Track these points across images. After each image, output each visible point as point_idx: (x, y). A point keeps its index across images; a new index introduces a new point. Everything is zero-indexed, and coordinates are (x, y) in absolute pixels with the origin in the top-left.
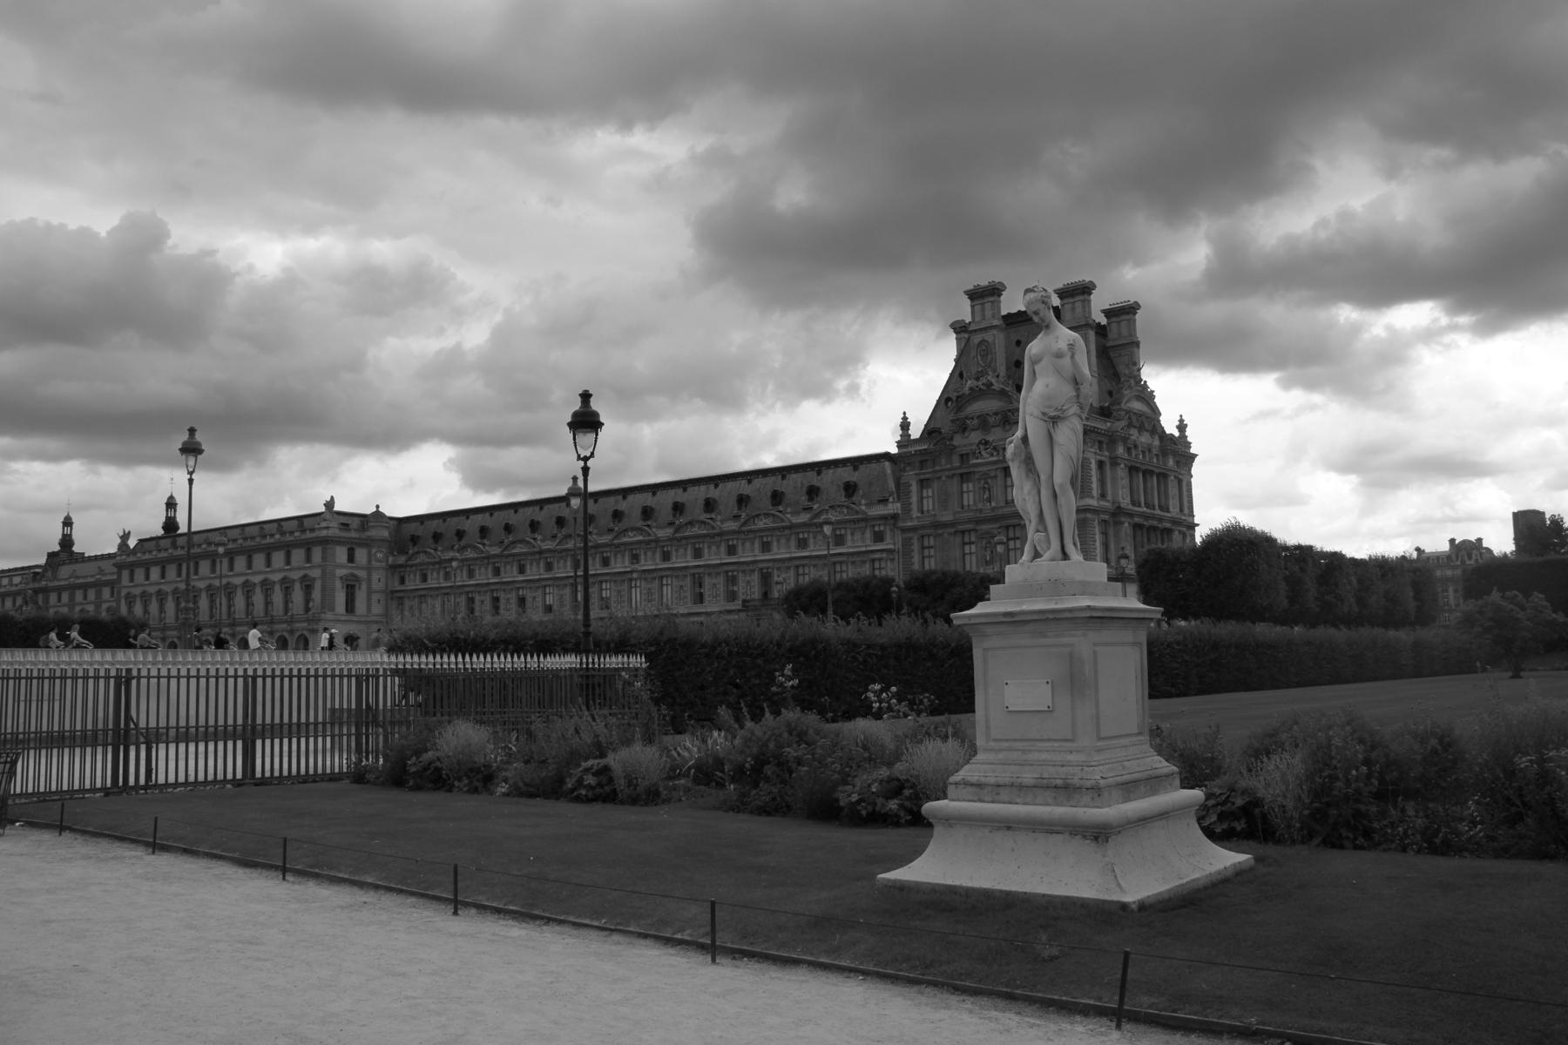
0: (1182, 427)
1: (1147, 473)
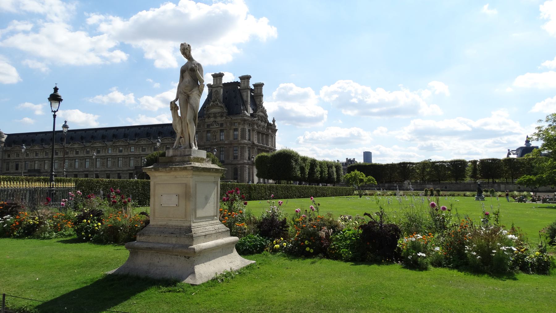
0: (274, 121)
1: (263, 134)
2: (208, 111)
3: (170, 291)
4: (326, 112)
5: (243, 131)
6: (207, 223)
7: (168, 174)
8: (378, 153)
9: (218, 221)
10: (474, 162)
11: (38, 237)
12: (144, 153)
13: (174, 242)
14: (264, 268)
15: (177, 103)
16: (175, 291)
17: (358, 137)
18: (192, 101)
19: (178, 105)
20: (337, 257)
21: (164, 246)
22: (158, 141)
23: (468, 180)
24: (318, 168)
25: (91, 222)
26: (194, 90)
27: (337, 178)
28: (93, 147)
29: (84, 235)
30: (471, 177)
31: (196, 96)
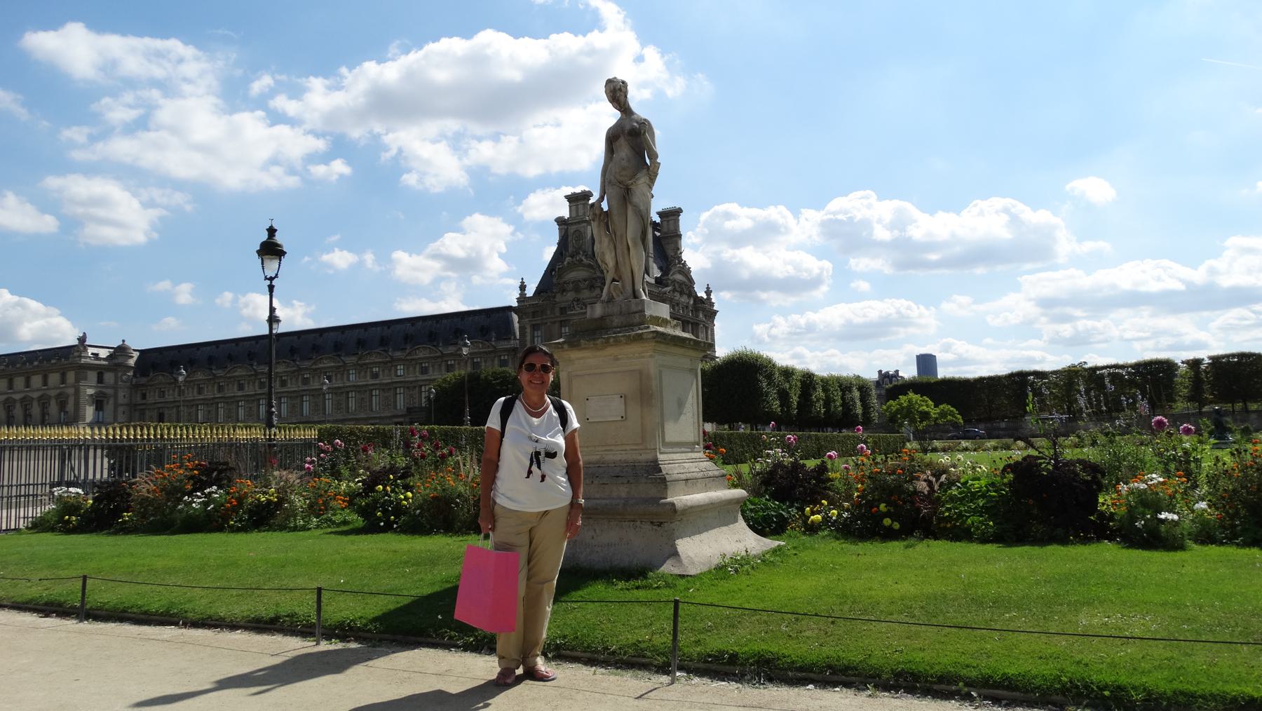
0: (708, 292)
2: (560, 276)
3: (638, 588)
4: (827, 264)
6: (683, 456)
7: (600, 353)
8: (949, 356)
9: (701, 455)
10: (1195, 364)
11: (283, 528)
12: (425, 377)
13: (623, 495)
14: (806, 556)
16: (645, 587)
17: (903, 321)
18: (636, 199)
20: (960, 534)
21: (604, 502)
22: (465, 345)
23: (1180, 406)
24: (820, 392)
25: (393, 491)
26: (639, 175)
27: (864, 414)
28: (315, 370)
29: (377, 517)
30: (1191, 399)
31: (645, 188)
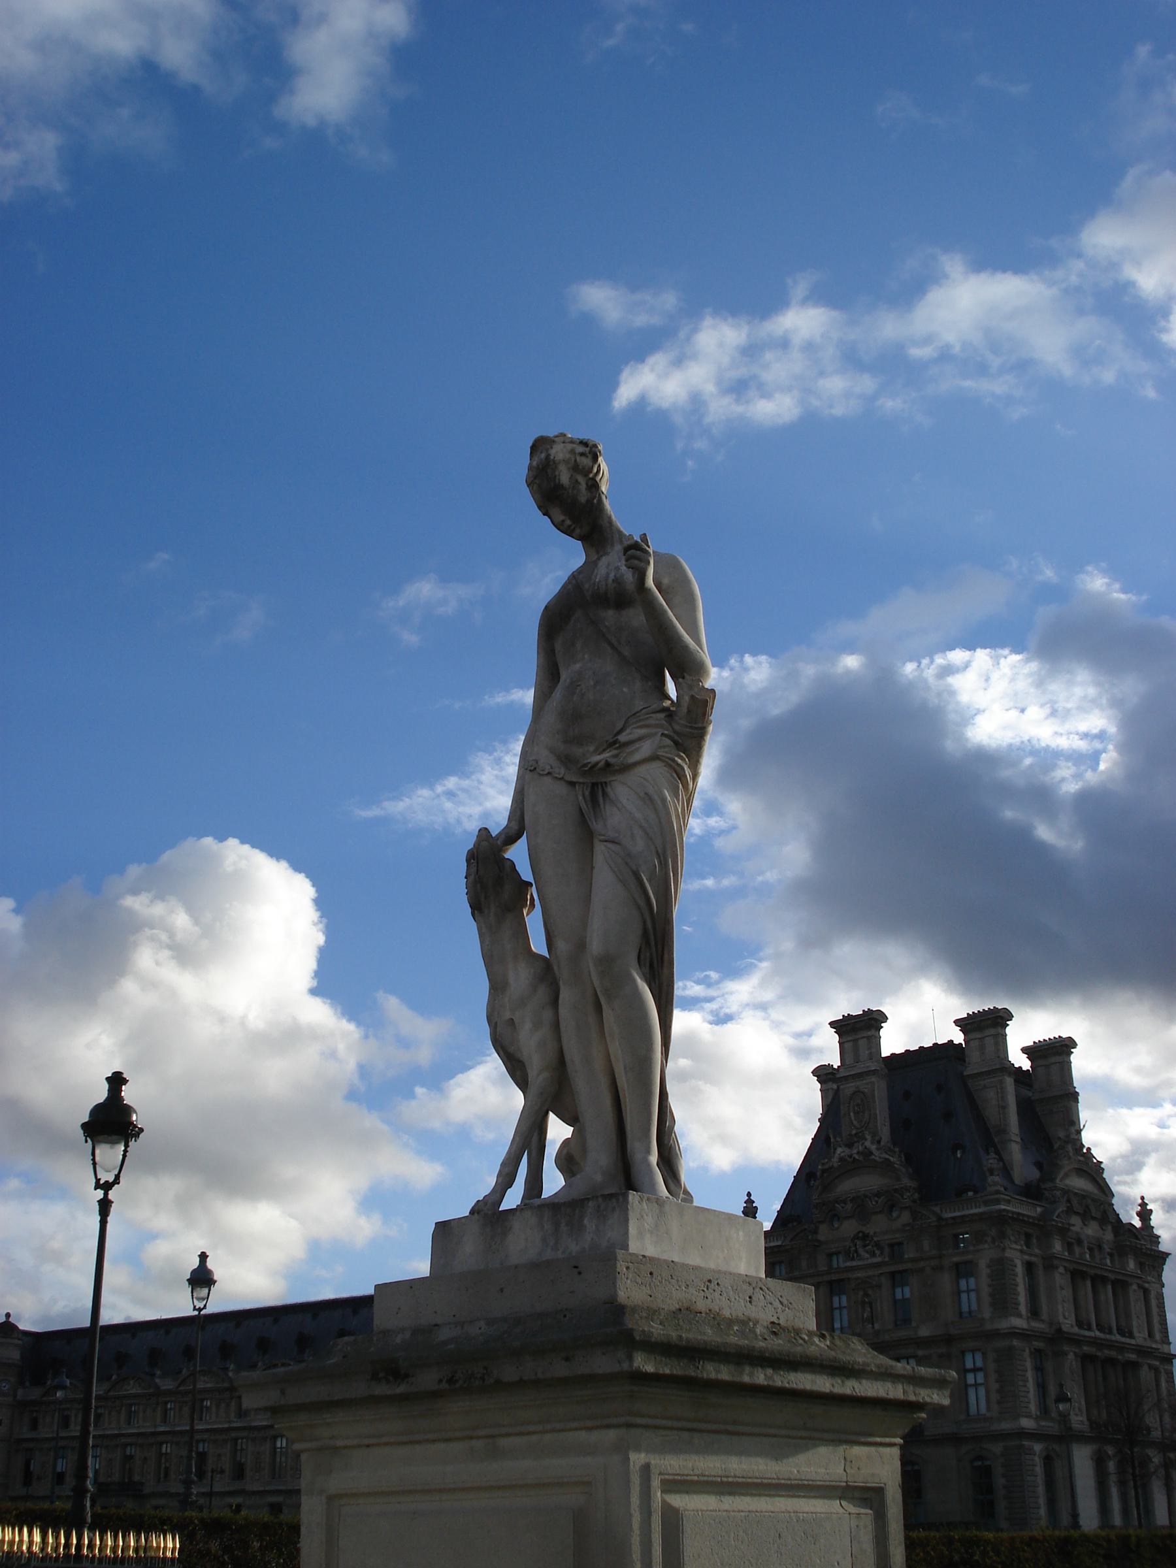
1: (1098, 1281)
5: (1000, 1269)
15: (518, 854)
19: (526, 874)
